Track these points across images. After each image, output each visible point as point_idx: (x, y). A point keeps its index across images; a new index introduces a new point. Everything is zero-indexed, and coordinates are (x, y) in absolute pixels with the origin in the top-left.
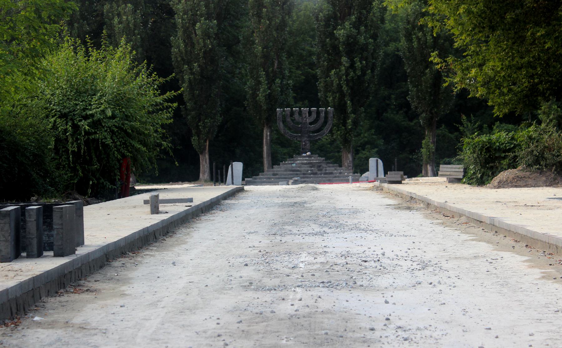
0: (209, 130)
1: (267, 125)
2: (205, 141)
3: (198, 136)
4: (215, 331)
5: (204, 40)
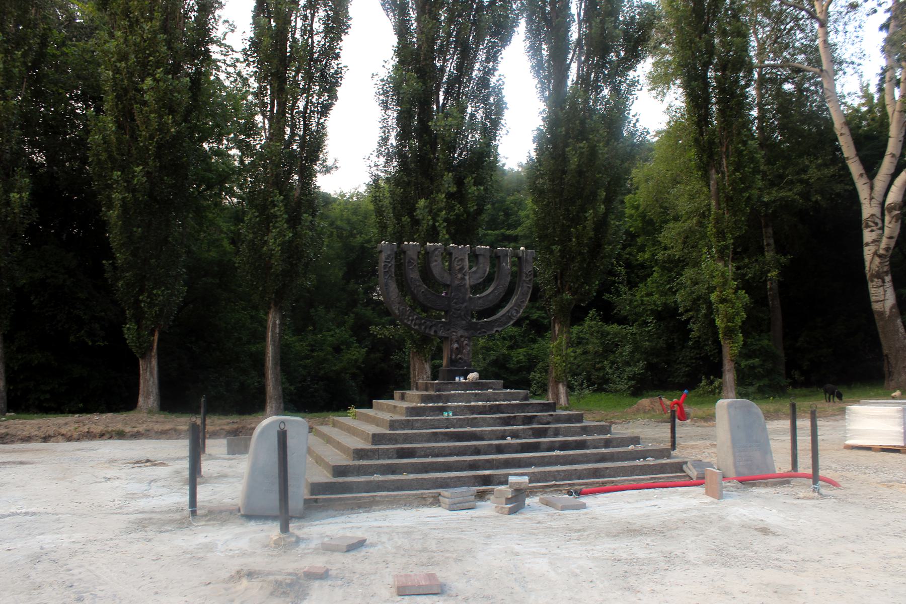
0: (161, 310)
1: (275, 305)
2: (152, 333)
3: (138, 322)
4: (153, 515)
5: (161, 117)
